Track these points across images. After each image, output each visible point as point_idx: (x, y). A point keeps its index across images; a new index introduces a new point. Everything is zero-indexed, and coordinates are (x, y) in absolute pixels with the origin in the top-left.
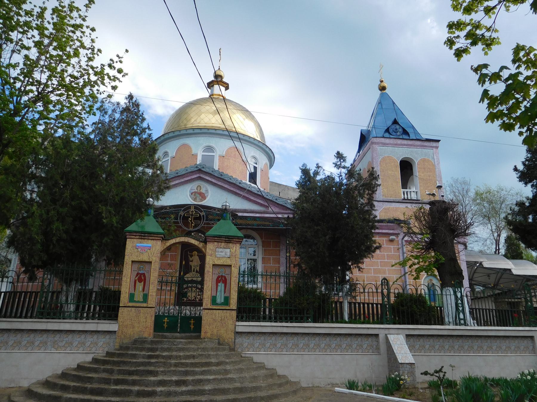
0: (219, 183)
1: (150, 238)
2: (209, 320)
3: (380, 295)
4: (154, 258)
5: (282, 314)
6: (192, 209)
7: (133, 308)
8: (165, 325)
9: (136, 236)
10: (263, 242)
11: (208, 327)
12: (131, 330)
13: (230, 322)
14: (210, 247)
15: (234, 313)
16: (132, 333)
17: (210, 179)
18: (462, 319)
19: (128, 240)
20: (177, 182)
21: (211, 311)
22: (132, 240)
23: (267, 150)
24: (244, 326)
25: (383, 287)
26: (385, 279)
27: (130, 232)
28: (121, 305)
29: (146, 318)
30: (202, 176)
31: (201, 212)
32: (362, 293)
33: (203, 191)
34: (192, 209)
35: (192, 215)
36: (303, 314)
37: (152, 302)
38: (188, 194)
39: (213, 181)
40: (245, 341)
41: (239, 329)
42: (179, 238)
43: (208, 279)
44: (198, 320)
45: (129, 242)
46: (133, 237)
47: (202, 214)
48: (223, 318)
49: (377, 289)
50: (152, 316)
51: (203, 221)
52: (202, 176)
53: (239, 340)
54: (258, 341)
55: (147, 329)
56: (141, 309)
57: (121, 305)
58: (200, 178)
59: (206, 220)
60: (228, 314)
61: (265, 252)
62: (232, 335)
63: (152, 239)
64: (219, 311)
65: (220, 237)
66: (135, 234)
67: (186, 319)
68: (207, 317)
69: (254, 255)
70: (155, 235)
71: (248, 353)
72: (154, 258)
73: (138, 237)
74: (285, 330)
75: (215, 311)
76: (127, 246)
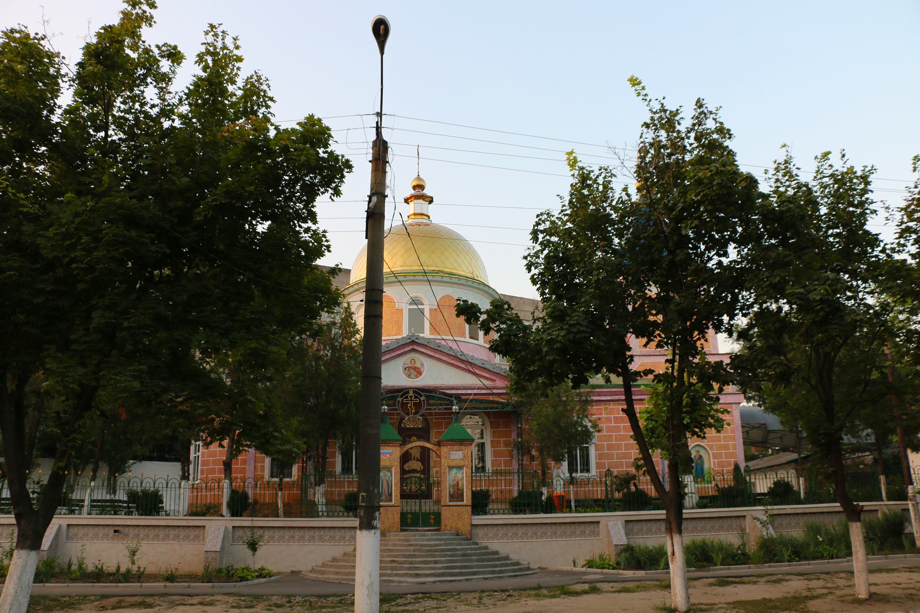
0: (437, 355)
3: (603, 485)
6: (411, 394)
8: (409, 521)
10: (491, 422)
13: (467, 516)
14: (444, 450)
15: (470, 509)
17: (425, 351)
23: (490, 291)
24: (479, 519)
30: (415, 347)
33: (418, 365)
34: (411, 394)
38: (401, 369)
39: (429, 353)
40: (480, 532)
41: (474, 522)
44: (438, 515)
52: (415, 347)
53: (475, 531)
54: (491, 532)
58: (414, 350)
61: (494, 434)
62: (469, 527)
65: (453, 440)
67: (426, 515)
68: (446, 513)
69: (482, 438)
71: (484, 542)
74: (807, 511)
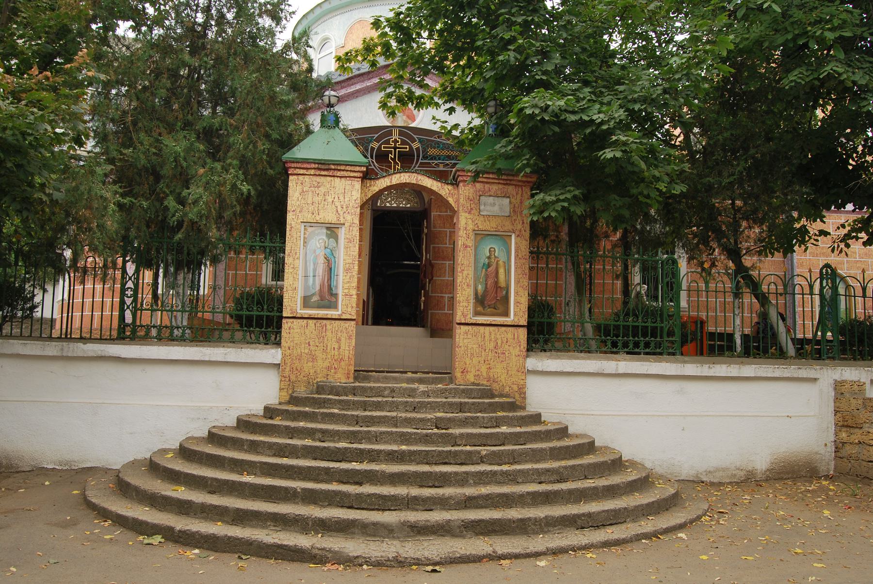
1: (339, 174)
2: (470, 346)
4: (349, 218)
5: (617, 336)
6: (395, 136)
7: (310, 321)
9: (307, 169)
11: (468, 361)
12: (310, 364)
15: (523, 333)
16: (312, 371)
18: (128, 325)
19: (291, 178)
20: (358, 87)
21: (475, 328)
22: (301, 177)
25: (824, 282)
26: (827, 266)
27: (297, 161)
28: (285, 315)
29: (339, 341)
31: (413, 141)
32: (781, 294)
34: (395, 136)
35: (395, 148)
36: (661, 337)
37: (349, 309)
42: (398, 176)
43: (466, 262)
45: (292, 181)
46: (302, 171)
47: (415, 146)
48: (499, 342)
49: (811, 287)
50: (350, 337)
51: (418, 160)
55: (343, 363)
56: (328, 322)
57: (285, 315)
59: (425, 158)
60: (510, 336)
63: (341, 177)
64: (492, 328)
66: (305, 166)
70: (348, 168)
72: (349, 218)
73: (312, 172)
75: (482, 328)
76: (290, 192)
